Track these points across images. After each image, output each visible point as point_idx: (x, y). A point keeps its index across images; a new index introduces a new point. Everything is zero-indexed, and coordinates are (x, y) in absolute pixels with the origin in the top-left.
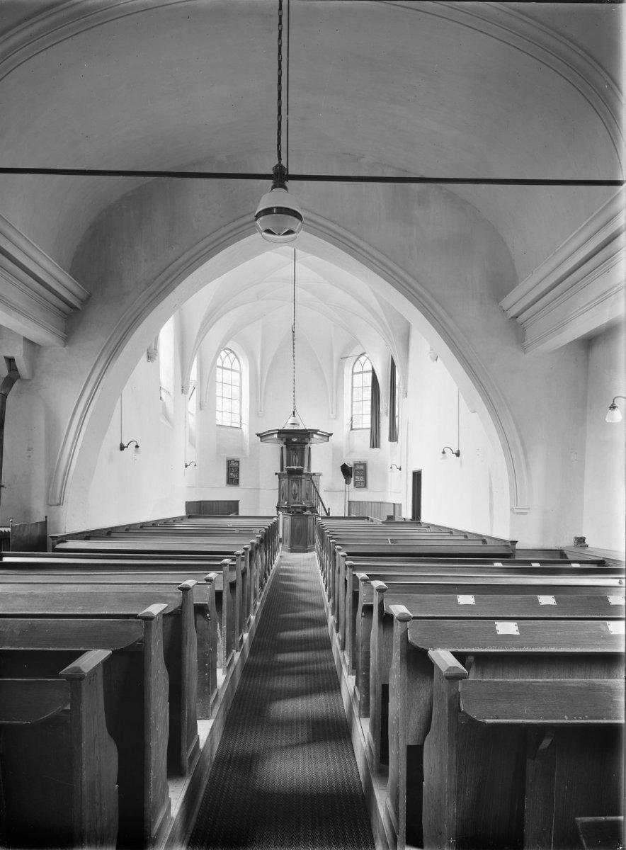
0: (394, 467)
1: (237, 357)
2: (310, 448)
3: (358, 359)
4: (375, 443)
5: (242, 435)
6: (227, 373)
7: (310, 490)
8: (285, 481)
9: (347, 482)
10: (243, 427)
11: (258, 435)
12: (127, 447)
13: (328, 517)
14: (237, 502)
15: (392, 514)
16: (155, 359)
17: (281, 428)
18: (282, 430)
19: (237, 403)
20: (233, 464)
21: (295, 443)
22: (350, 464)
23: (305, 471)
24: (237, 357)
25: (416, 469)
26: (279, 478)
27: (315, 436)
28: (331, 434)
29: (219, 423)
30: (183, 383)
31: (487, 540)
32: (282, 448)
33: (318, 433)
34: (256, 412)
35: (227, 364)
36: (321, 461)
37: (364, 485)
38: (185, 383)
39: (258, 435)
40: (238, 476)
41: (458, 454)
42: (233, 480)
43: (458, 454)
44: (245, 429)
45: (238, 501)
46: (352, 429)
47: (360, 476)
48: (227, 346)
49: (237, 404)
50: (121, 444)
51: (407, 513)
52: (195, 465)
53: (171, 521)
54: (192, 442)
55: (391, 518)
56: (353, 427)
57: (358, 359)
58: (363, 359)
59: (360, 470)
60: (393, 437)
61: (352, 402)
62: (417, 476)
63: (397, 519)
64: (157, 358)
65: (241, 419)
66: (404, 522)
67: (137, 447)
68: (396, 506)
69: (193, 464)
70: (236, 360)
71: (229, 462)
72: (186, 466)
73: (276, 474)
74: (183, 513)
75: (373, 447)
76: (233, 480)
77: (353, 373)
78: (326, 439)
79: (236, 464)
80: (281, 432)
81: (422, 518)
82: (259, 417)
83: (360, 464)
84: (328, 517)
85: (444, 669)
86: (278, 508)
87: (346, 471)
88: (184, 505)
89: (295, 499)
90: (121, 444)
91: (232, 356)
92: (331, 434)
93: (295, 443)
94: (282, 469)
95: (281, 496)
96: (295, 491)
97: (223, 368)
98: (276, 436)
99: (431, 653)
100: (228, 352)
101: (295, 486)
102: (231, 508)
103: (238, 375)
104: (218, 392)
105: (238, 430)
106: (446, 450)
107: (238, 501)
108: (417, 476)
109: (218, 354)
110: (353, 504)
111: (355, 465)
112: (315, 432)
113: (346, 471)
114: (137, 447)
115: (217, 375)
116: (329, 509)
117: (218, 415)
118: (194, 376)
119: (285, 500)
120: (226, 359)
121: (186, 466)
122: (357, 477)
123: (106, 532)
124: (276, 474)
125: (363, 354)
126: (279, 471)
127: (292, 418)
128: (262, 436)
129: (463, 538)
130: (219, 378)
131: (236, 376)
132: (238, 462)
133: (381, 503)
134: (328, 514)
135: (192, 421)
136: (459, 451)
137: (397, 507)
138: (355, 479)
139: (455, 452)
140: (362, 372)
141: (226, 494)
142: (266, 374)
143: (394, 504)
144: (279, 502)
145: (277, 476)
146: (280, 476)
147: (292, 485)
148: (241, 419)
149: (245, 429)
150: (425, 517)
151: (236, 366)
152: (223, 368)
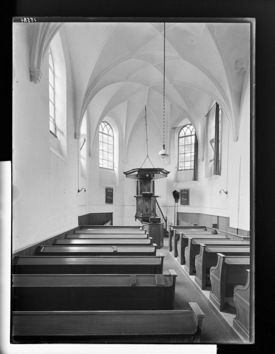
1: (111, 128)
2: (154, 181)
4: (195, 178)
5: (114, 174)
6: (105, 136)
7: (155, 206)
8: (141, 201)
9: (176, 201)
10: (115, 169)
11: (124, 173)
12: (81, 191)
16: (38, 79)
17: (140, 168)
19: (111, 147)
20: (109, 191)
21: (146, 177)
22: (178, 191)
24: (111, 128)
26: (137, 199)
28: (169, 172)
30: (75, 130)
32: (138, 181)
33: (163, 171)
34: (123, 160)
35: (105, 131)
36: (161, 188)
37: (186, 203)
38: (77, 131)
39: (124, 173)
40: (112, 198)
41: (227, 193)
42: (109, 199)
43: (227, 193)
44: (116, 170)
46: (178, 170)
47: (184, 198)
48: (104, 120)
56: (180, 169)
57: (182, 129)
59: (185, 194)
60: (217, 171)
65: (114, 165)
67: (85, 191)
69: (84, 189)
70: (111, 129)
71: (107, 189)
72: (79, 191)
73: (135, 197)
75: (195, 180)
76: (109, 199)
77: (179, 138)
78: (166, 175)
79: (111, 191)
80: (140, 170)
81: (230, 225)
82: (124, 163)
83: (185, 190)
89: (147, 211)
91: (108, 126)
92: (169, 172)
94: (138, 194)
95: (138, 210)
96: (147, 207)
97: (103, 133)
100: (106, 124)
101: (147, 203)
102: (109, 217)
104: (101, 148)
105: (113, 171)
109: (99, 123)
110: (180, 214)
111: (181, 191)
113: (176, 195)
114: (85, 191)
115: (100, 138)
116: (166, 217)
117: (101, 162)
118: (83, 130)
119: (141, 213)
121: (79, 191)
124: (135, 197)
127: (163, 150)
128: (127, 174)
130: (100, 139)
131: (110, 138)
132: (112, 190)
135: (84, 162)
138: (181, 199)
141: (106, 209)
142: (127, 143)
143: (218, 217)
144: (137, 213)
145: (136, 198)
146: (138, 198)
147: (145, 203)
148: (114, 165)
149: (116, 170)
151: (110, 133)
152: (103, 133)
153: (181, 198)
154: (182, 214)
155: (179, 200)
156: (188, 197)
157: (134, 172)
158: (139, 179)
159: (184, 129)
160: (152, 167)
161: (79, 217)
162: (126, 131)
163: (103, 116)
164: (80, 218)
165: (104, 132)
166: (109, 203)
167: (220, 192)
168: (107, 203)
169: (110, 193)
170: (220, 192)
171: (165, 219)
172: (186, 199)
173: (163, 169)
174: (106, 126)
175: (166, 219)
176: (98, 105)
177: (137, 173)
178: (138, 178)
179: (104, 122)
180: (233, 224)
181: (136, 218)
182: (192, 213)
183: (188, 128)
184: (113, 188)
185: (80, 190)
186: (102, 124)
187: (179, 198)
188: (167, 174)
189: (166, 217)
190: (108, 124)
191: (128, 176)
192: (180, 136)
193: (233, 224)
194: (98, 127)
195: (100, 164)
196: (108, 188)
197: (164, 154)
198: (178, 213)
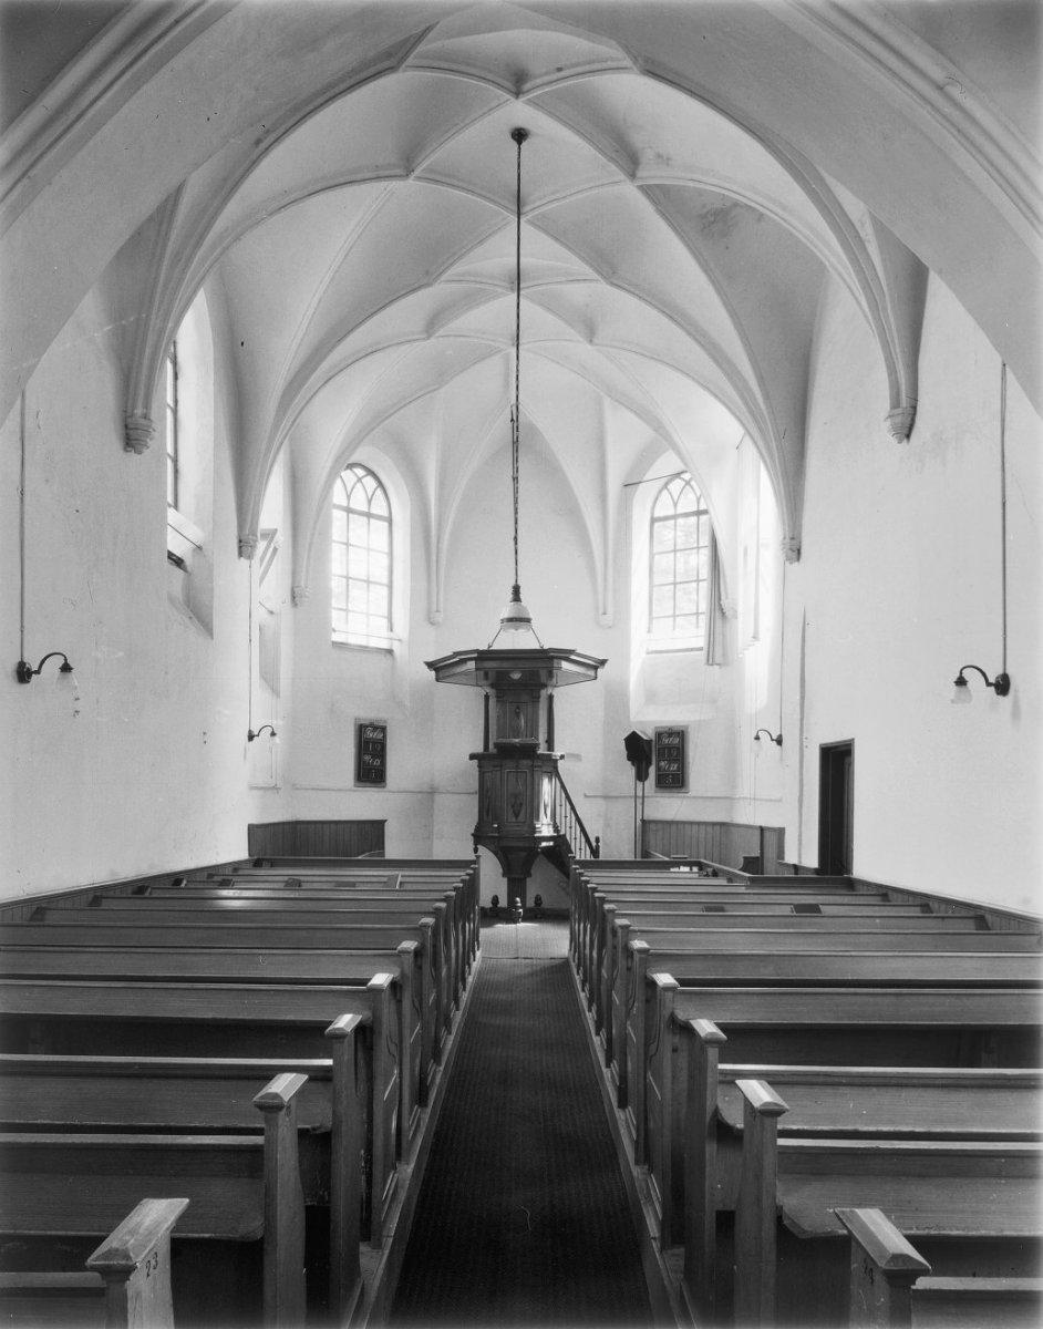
0: (973, 678)
1: (380, 484)
2: (551, 698)
3: (666, 484)
9: (641, 776)
11: (430, 665)
12: (38, 672)
13: (597, 864)
14: (379, 826)
15: (756, 853)
17: (484, 647)
18: (489, 652)
20: (370, 734)
21: (517, 683)
22: (647, 733)
23: (542, 750)
24: (380, 484)
25: (834, 737)
26: (479, 766)
27: (565, 665)
28: (603, 662)
29: (336, 637)
30: (293, 582)
31: (988, 917)
32: (487, 697)
33: (573, 657)
34: (430, 615)
35: (359, 502)
36: (581, 732)
37: (674, 780)
39: (430, 665)
40: (383, 763)
41: (779, 741)
43: (779, 741)
45: (382, 823)
47: (670, 762)
48: (354, 459)
49: (371, 589)
50: (22, 665)
51: (804, 850)
52: (273, 734)
53: (228, 871)
54: (269, 677)
55: (753, 864)
58: (676, 485)
61: (651, 586)
62: (836, 762)
63: (771, 870)
64: (156, 434)
66: (797, 878)
67: (66, 668)
68: (767, 834)
70: (379, 492)
71: (361, 729)
72: (251, 737)
74: (235, 849)
77: (653, 520)
78: (592, 673)
79: (378, 735)
80: (483, 656)
84: (597, 864)
85: (702, 1035)
86: (479, 837)
87: (638, 750)
88: (246, 828)
89: (517, 816)
90: (22, 665)
91: (370, 482)
92: (603, 662)
93: (517, 683)
98: (471, 665)
99: (692, 1022)
100: (360, 472)
102: (370, 835)
103: (386, 524)
106: (967, 674)
107: (382, 823)
108: (836, 762)
109: (333, 474)
111: (659, 735)
112: (565, 655)
113: (638, 750)
114: (66, 668)
116: (597, 840)
117: (336, 618)
118: (272, 510)
120: (350, 490)
121: (251, 737)
122: (662, 764)
123: (91, 896)
125: (678, 475)
126: (480, 749)
128: (441, 668)
129: (916, 912)
132: (383, 729)
133: (722, 824)
134: (595, 852)
136: (781, 736)
137: (770, 839)
138: (658, 769)
139: (775, 737)
140: (674, 517)
141: (360, 805)
143: (762, 829)
150: (865, 866)
152: (349, 510)
153: (658, 762)
154: (660, 826)
155: (652, 770)
156: (683, 758)
157: (464, 661)
158: (492, 686)
159: (670, 486)
160: (536, 646)
161: (251, 828)
162: (442, 485)
163: (353, 443)
164: (253, 830)
165: (352, 506)
166: (368, 784)
167: (757, 738)
168: (361, 784)
169: (375, 742)
170: (757, 738)
171: (594, 844)
172: (674, 767)
173: (572, 652)
174: (360, 480)
175: (598, 847)
176: (333, 417)
177: (471, 665)
178: (490, 682)
179: (350, 466)
180: (791, 857)
181: (476, 843)
182: (699, 823)
183: (688, 483)
184: (385, 722)
185: (35, 668)
186: (347, 475)
187: (651, 764)
188: (596, 668)
189: (597, 840)
190: (371, 472)
191: (444, 678)
192: (656, 515)
193: (791, 857)
194: (329, 486)
195: (334, 631)
196: (367, 723)
197: (511, 616)
198: (643, 821)
